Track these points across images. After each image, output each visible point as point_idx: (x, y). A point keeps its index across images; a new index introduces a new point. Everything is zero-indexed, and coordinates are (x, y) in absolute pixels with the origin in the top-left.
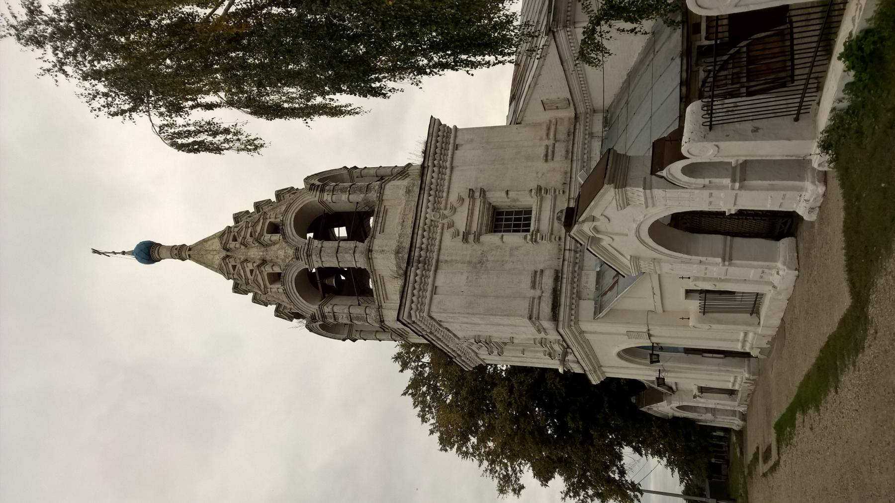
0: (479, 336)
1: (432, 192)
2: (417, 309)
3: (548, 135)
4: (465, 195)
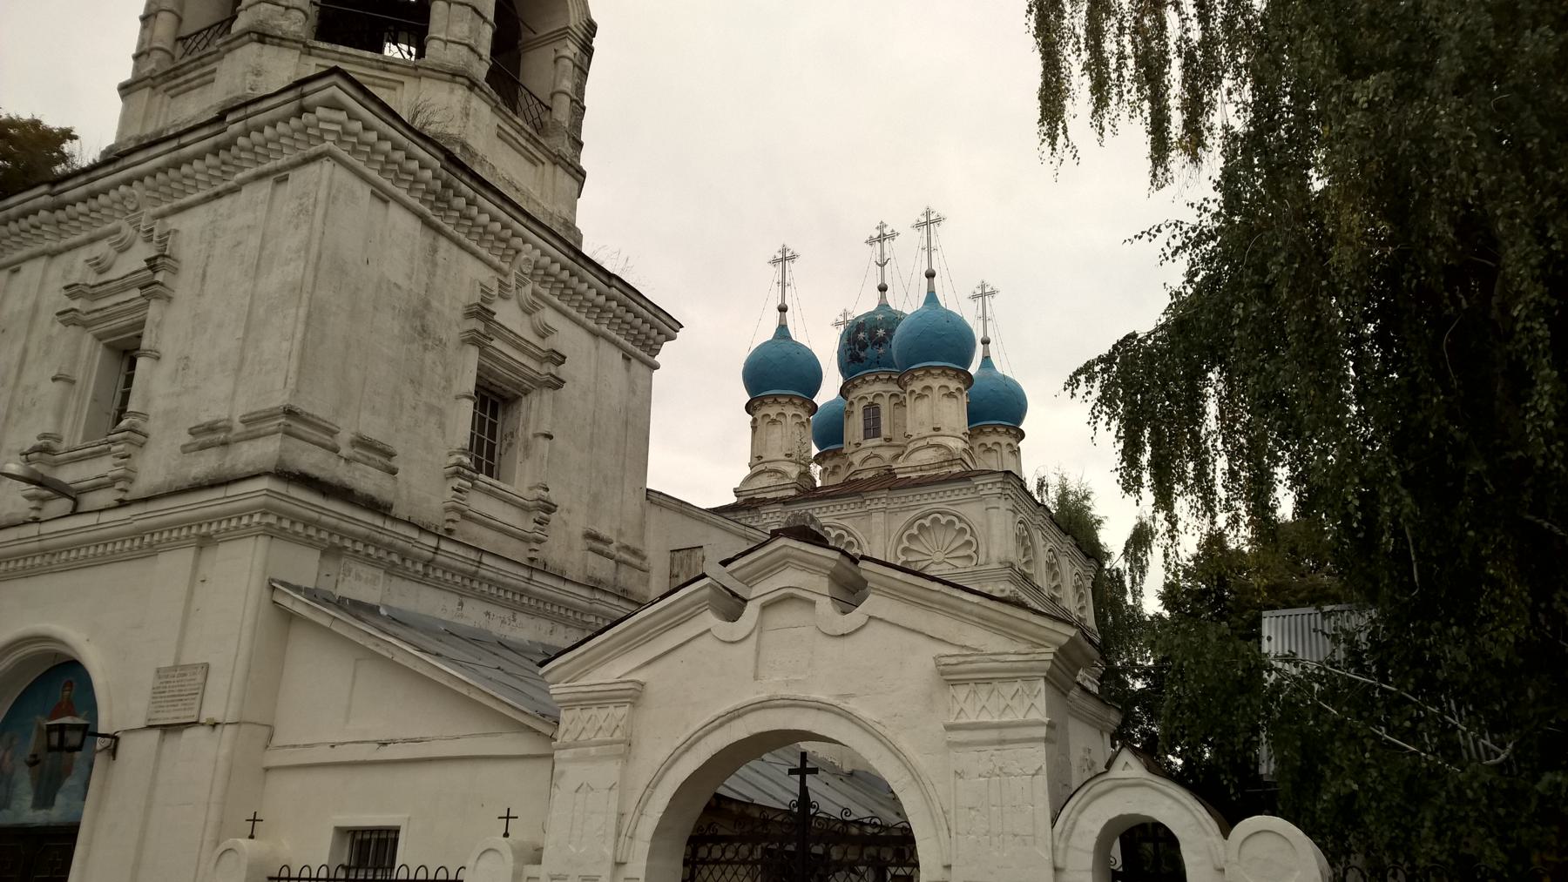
0: (175, 271)
1: (566, 273)
2: (346, 132)
3: (627, 548)
4: (552, 342)
